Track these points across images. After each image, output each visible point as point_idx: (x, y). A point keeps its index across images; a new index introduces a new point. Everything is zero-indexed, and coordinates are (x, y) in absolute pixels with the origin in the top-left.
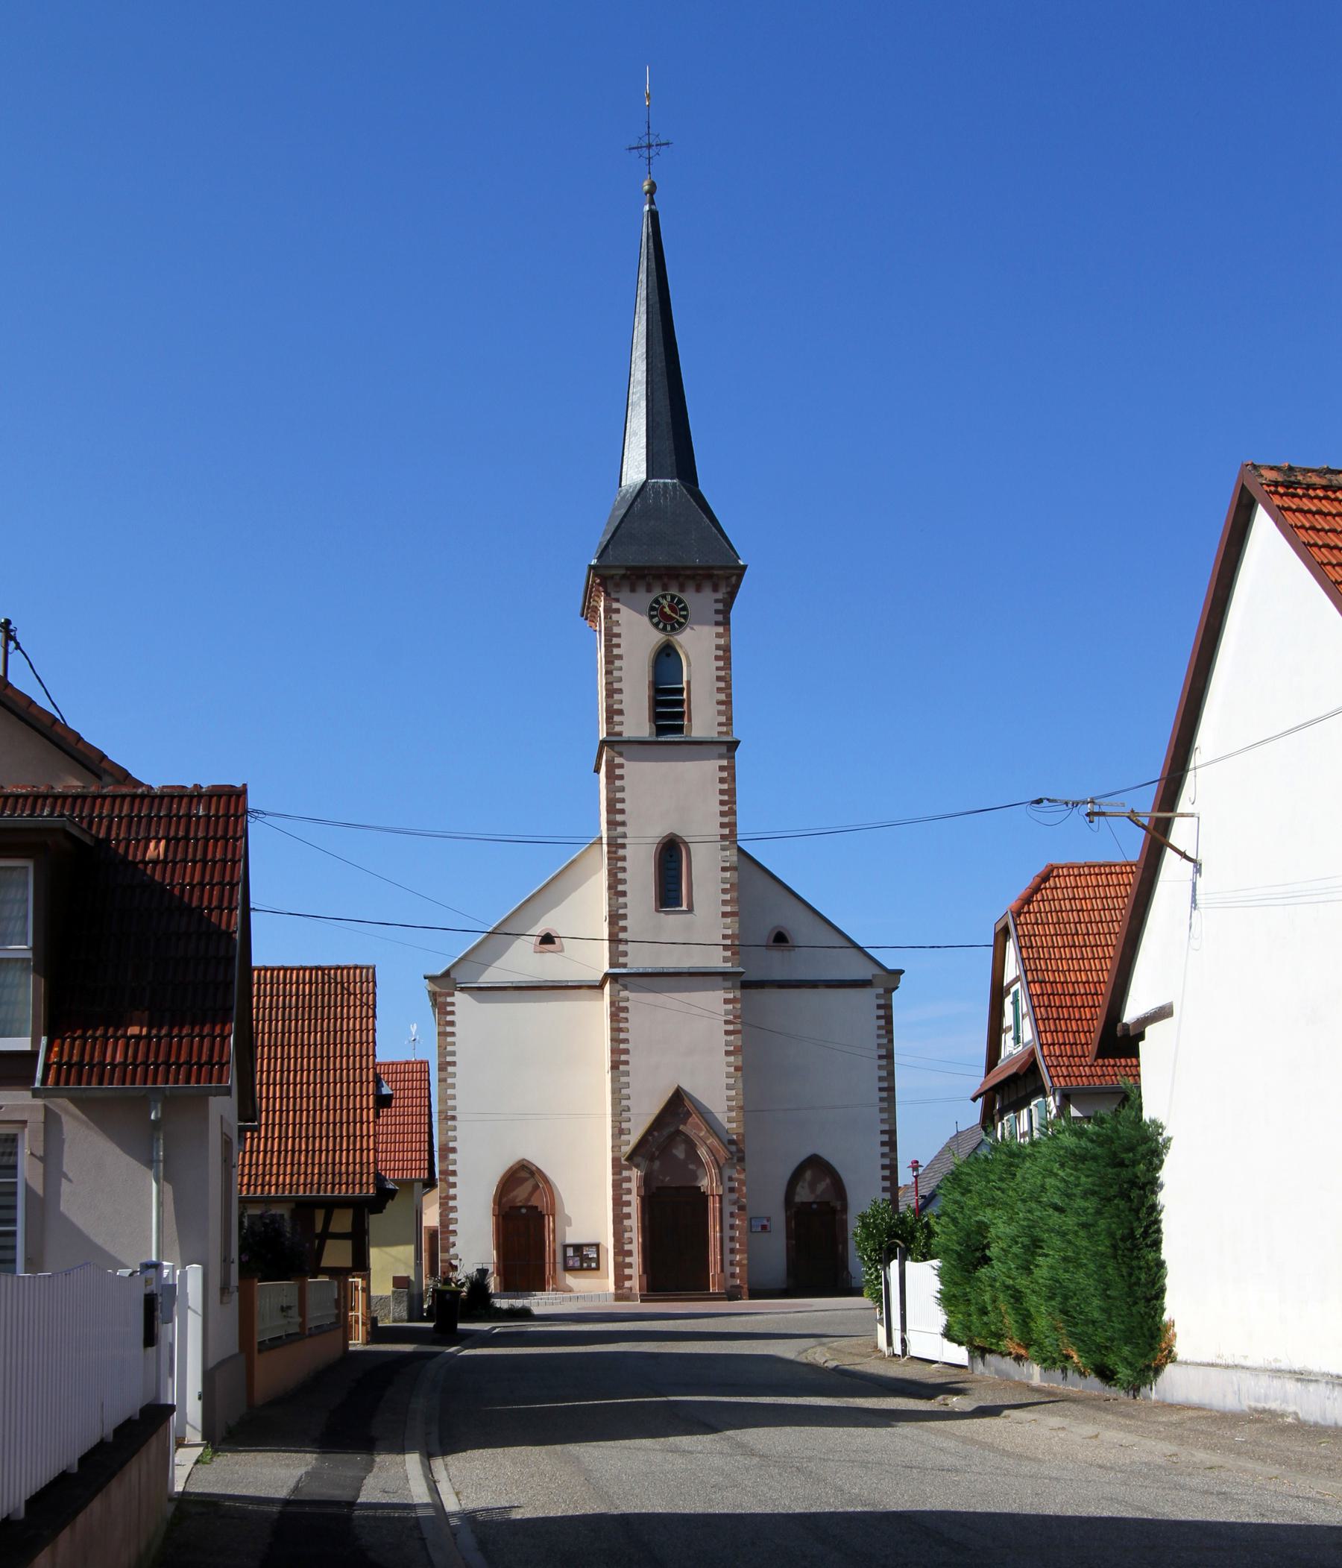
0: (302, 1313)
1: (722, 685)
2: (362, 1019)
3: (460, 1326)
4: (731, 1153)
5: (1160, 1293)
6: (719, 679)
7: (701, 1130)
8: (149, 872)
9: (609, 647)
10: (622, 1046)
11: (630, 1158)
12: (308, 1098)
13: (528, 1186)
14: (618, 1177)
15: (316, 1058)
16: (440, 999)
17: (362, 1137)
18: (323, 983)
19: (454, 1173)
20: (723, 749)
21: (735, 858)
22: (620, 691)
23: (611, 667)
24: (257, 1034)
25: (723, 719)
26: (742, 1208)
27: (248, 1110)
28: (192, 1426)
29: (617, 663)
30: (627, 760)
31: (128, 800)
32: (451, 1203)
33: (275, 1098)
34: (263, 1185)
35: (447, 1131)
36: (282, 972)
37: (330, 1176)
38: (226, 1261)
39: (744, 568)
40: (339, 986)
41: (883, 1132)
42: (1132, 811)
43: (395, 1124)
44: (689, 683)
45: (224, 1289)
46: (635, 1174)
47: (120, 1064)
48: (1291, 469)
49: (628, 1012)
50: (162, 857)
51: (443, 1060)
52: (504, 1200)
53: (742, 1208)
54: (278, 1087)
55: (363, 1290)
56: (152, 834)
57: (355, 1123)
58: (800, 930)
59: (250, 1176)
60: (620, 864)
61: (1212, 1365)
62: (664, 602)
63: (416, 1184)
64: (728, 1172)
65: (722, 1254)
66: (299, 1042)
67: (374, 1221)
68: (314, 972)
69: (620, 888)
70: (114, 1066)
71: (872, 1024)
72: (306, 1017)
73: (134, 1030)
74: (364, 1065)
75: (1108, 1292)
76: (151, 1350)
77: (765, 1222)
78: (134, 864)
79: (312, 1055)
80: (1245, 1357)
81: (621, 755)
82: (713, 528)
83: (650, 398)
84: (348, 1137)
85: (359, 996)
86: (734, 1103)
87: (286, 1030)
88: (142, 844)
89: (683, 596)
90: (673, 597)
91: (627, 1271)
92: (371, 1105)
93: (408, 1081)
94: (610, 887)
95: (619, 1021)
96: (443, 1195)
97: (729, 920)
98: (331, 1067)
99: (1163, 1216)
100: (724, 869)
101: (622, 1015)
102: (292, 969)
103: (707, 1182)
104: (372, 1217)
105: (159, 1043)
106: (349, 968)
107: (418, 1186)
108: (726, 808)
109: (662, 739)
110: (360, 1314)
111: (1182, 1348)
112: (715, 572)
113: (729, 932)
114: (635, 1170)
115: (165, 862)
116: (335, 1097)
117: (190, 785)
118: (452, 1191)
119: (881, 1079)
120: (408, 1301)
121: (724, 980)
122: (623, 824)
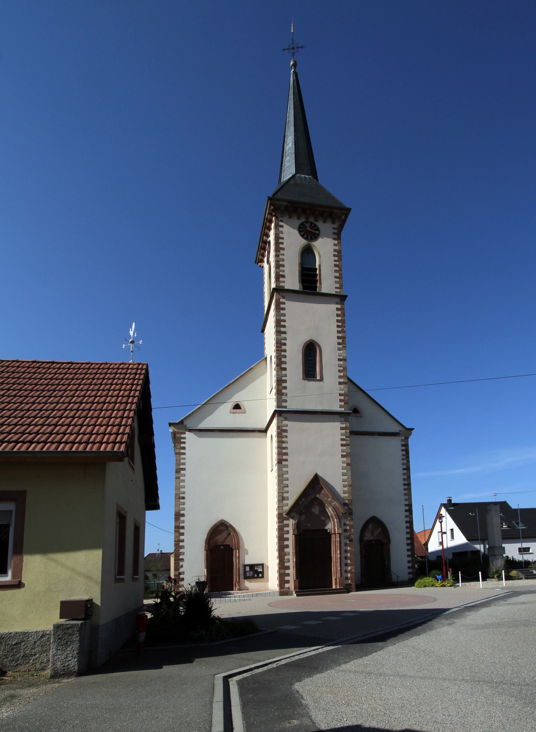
7: (329, 498)
10: (284, 451)
11: (289, 513)
13: (225, 534)
14: (281, 524)
16: (177, 436)
19: (183, 528)
23: (278, 253)
29: (282, 252)
30: (287, 300)
35: (180, 505)
41: (406, 505)
46: (291, 522)
49: (287, 432)
51: (178, 467)
52: (211, 542)
60: (283, 353)
64: (343, 521)
65: (341, 567)
69: (283, 366)
81: (284, 297)
91: (287, 578)
95: (282, 437)
96: (177, 540)
97: (342, 386)
101: (284, 434)
108: (340, 329)
113: (343, 392)
120: (80, 641)
122: (285, 333)
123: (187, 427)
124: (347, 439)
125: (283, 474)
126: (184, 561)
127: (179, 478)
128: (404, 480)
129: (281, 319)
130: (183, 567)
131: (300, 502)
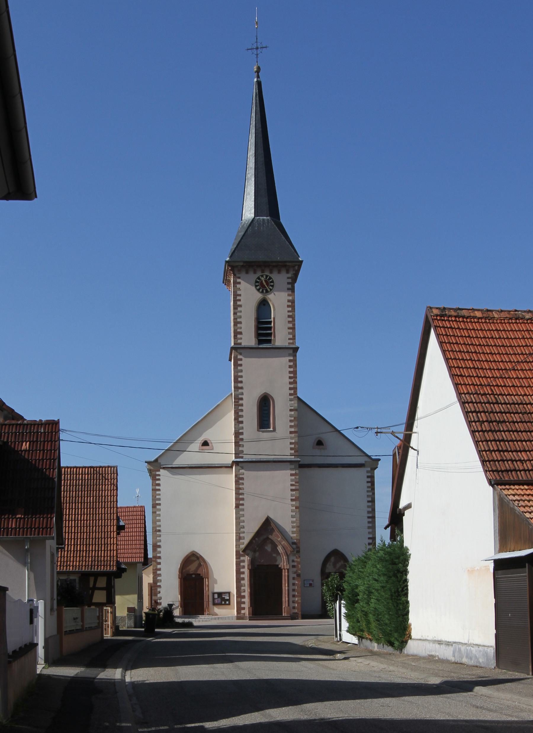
0: (82, 621)
1: (291, 319)
2: (111, 491)
3: (156, 630)
4: (293, 549)
5: (408, 613)
6: (289, 316)
7: (279, 537)
8: (23, 454)
9: (235, 301)
10: (241, 497)
11: (244, 551)
12: (87, 527)
14: (238, 560)
15: (90, 509)
17: (111, 544)
18: (94, 474)
19: (160, 558)
20: (291, 351)
21: (296, 405)
22: (240, 323)
24: (64, 504)
25: (291, 336)
26: (299, 575)
27: (60, 541)
28: (40, 658)
29: (239, 309)
31: (15, 426)
32: (158, 572)
33: (72, 527)
34: (67, 566)
36: (75, 469)
37: (96, 562)
38: (52, 599)
39: (302, 262)
40: (101, 475)
41: (369, 538)
42: (393, 431)
43: (125, 541)
44: (274, 318)
45: (52, 609)
46: (247, 559)
47: (14, 528)
48: (444, 308)
50: (28, 449)
52: (184, 571)
53: (299, 575)
54: (73, 522)
55: (111, 613)
56: (24, 440)
57: (108, 538)
58: (329, 439)
59: (61, 562)
60: (240, 408)
61: (420, 640)
62: (263, 279)
63: (138, 564)
64: (292, 558)
66: (83, 501)
67: (118, 582)
68: (89, 469)
69: (240, 419)
70: (12, 529)
71: (364, 485)
72: (86, 490)
73: (18, 516)
74: (112, 512)
75: (390, 613)
76: (32, 625)
77: (311, 582)
78: (17, 451)
79: (88, 507)
80: (428, 636)
81: (241, 354)
82: (287, 242)
83: (256, 176)
84: (105, 544)
85: (110, 480)
86: (295, 524)
87: (77, 496)
88: (20, 444)
89: (271, 276)
90: (267, 276)
91: (243, 606)
92: (115, 530)
93: (135, 515)
94: (235, 419)
95: (239, 485)
96: (154, 568)
98: (97, 513)
99: (409, 584)
100: (291, 410)
101: (241, 481)
102: (80, 468)
103: (283, 563)
104: (116, 580)
105: (28, 520)
106: (105, 467)
107: (140, 566)
108: (292, 380)
109: (261, 346)
110: (110, 623)
111: (414, 634)
112: (288, 264)
114: (247, 557)
115: (29, 451)
116: (99, 526)
117: (38, 420)
118: (159, 566)
119: (369, 512)
121: (291, 464)
123: (161, 464)
124: (296, 484)
125: (240, 517)
126: (161, 588)
127: (155, 512)
128: (369, 512)
129: (239, 375)
130: (160, 592)
131: (254, 541)
